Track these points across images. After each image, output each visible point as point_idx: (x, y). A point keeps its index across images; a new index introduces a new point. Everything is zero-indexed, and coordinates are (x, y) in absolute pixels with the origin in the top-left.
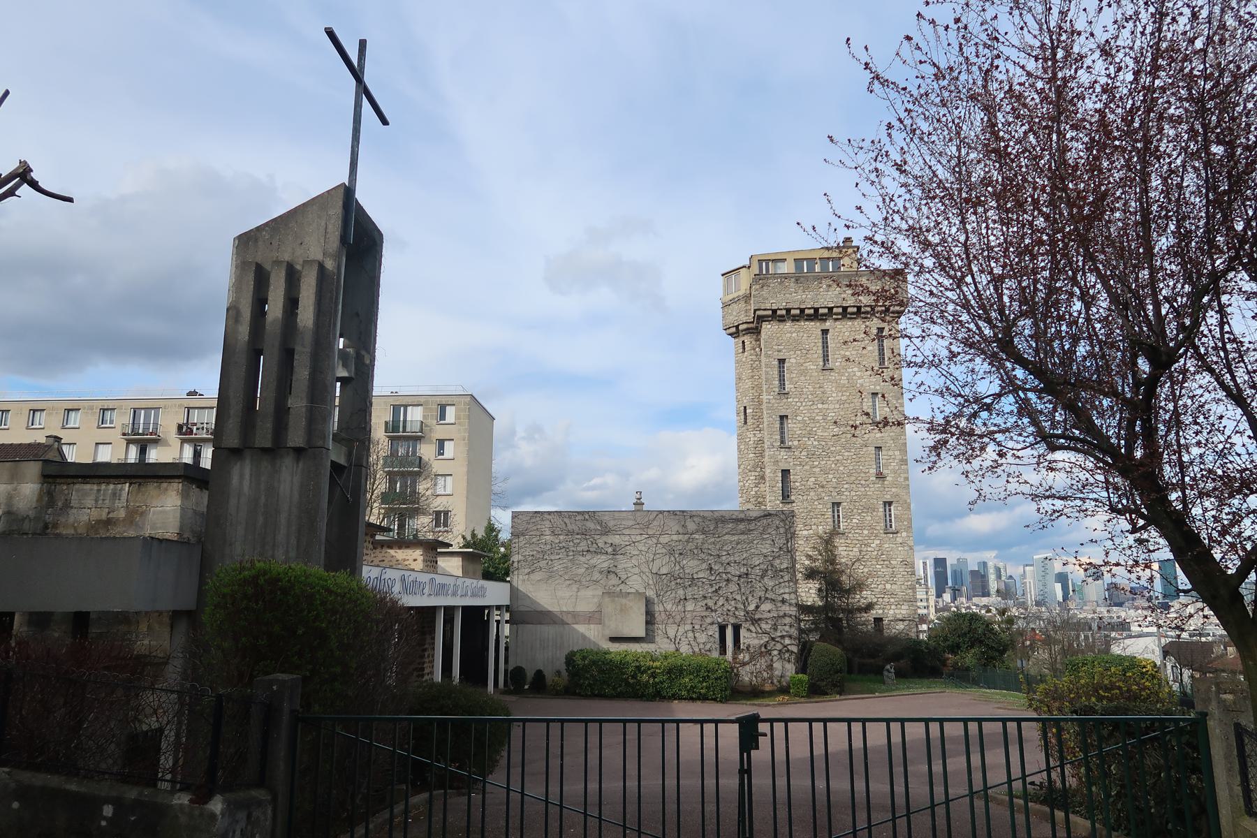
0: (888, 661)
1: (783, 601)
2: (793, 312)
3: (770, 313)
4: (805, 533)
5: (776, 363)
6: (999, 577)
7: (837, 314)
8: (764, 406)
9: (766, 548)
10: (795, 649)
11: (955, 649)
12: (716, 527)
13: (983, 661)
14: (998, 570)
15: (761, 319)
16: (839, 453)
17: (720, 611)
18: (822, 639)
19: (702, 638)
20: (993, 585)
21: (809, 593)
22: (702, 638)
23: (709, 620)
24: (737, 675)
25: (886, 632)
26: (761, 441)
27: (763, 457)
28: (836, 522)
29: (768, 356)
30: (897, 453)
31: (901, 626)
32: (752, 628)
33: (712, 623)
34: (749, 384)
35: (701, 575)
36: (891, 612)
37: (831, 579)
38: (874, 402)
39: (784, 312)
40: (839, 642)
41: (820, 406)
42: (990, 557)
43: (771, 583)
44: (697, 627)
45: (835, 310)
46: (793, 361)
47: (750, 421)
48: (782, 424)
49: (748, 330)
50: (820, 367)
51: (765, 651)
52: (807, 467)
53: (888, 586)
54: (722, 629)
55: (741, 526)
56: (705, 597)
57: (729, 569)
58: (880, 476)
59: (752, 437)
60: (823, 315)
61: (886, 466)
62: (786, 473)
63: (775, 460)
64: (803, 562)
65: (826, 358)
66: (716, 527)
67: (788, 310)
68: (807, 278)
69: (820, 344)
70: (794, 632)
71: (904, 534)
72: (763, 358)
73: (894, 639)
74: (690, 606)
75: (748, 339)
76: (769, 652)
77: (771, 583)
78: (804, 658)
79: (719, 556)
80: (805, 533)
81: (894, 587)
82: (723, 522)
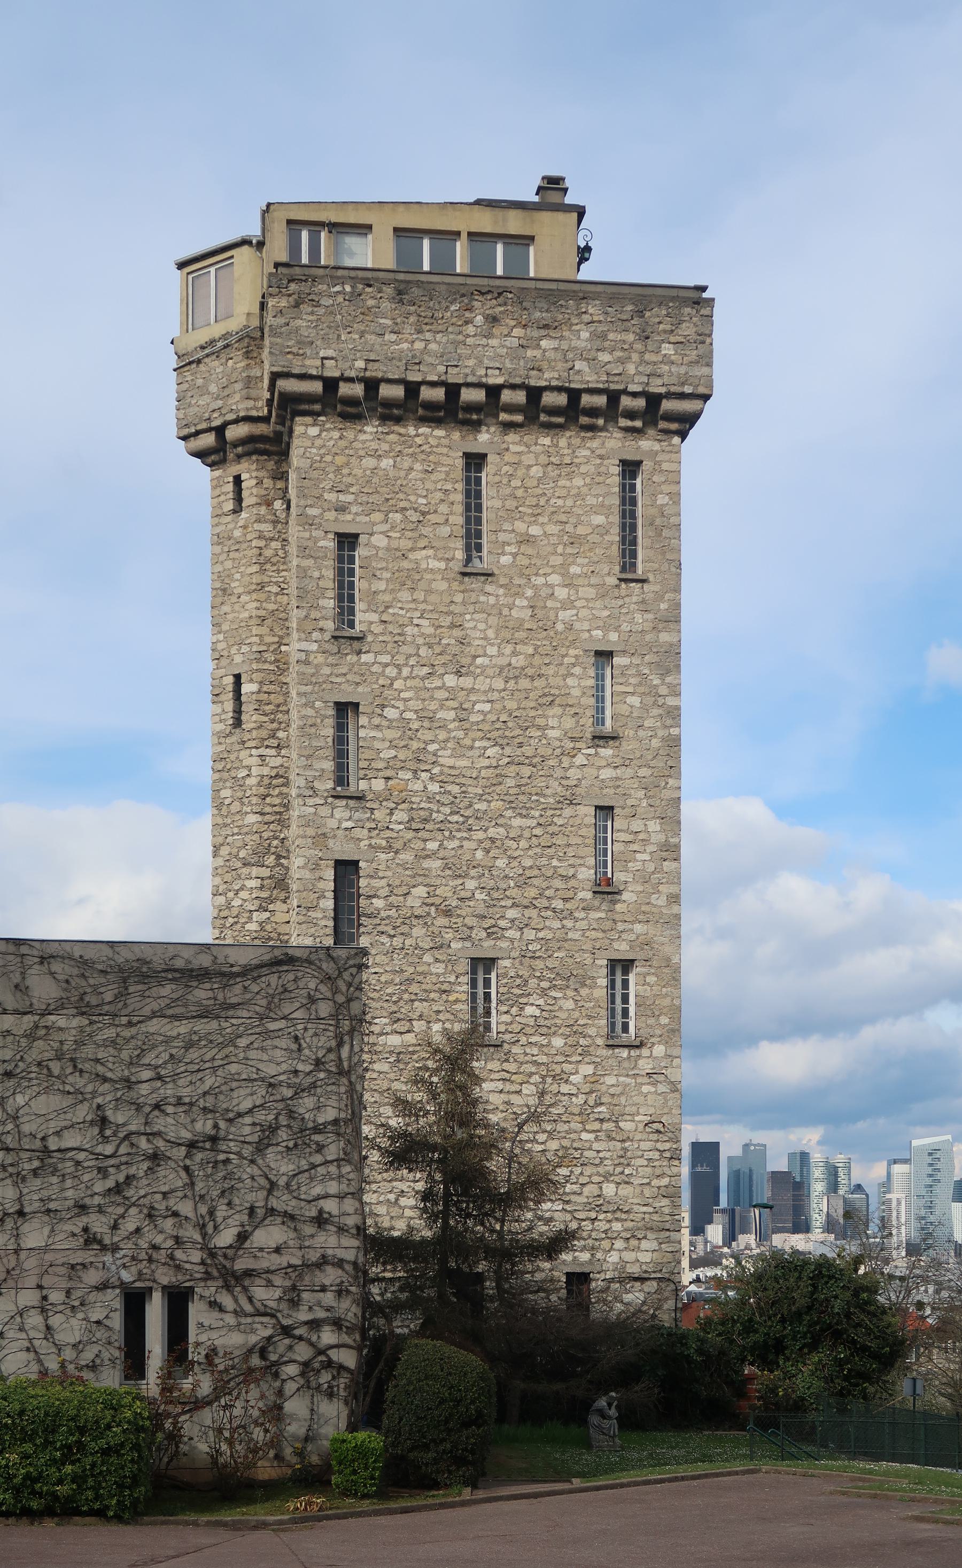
0: (602, 1387)
1: (321, 1220)
2: (386, 391)
3: (316, 387)
4: (394, 1040)
5: (329, 544)
6: (833, 1186)
7: (511, 408)
8: (291, 678)
9: (274, 1061)
10: (348, 1358)
11: (769, 1353)
12: (122, 995)
13: (839, 1383)
14: (832, 1173)
15: (289, 407)
16: (497, 819)
17: (127, 1249)
18: (429, 1328)
19: (70, 1329)
20: (819, 1206)
21: (397, 1203)
22: (70, 1329)
23: (92, 1277)
24: (174, 1437)
25: (597, 1311)
26: (281, 777)
27: (283, 823)
28: (480, 1007)
29: (308, 523)
30: (654, 826)
31: (635, 1296)
32: (226, 1300)
33: (103, 1287)
34: (250, 607)
35: (71, 1140)
36: (614, 1258)
37: (462, 1163)
38: (600, 677)
39: (358, 390)
40: (473, 1339)
41: (451, 680)
42: (809, 1138)
43: (286, 1167)
44: (56, 1297)
45: (507, 396)
46: (379, 541)
47: (250, 718)
48: (341, 727)
49: (247, 443)
50: (457, 566)
51: (261, 1365)
52: (407, 856)
53: (609, 1189)
54: (134, 1303)
55: (201, 994)
56: (82, 1208)
57: (160, 1123)
58: (606, 889)
59: (253, 766)
60: (472, 407)
61: (624, 861)
62: (346, 870)
63: (320, 828)
64: (381, 1118)
65: (473, 540)
66: (122, 995)
67: (372, 385)
68: (429, 290)
69: (459, 497)
70: (349, 1310)
71: (659, 1050)
72: (294, 531)
73: (621, 1329)
74: (34, 1235)
75: (249, 471)
76: (273, 1369)
77: (286, 1167)
78: (373, 1384)
79: (129, 1084)
80: (394, 1040)
81: (625, 1191)
82: (144, 978)
